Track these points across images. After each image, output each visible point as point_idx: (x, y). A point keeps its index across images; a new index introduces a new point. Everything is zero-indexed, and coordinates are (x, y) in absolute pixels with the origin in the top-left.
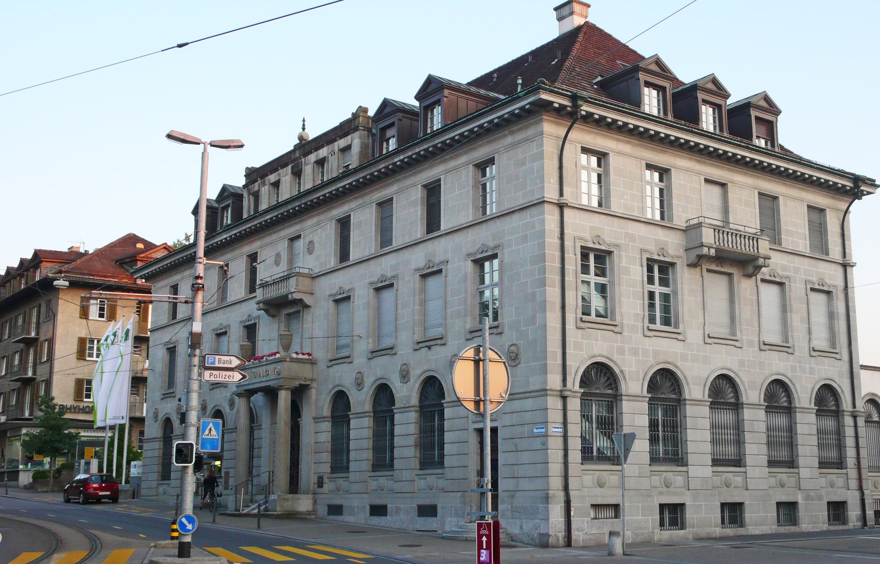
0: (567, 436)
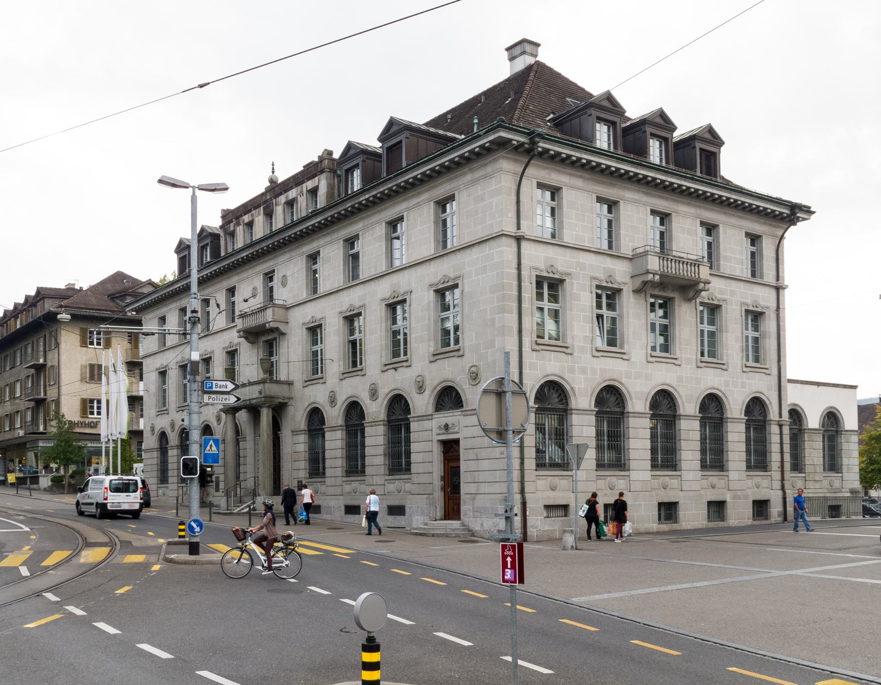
0: (524, 447)
